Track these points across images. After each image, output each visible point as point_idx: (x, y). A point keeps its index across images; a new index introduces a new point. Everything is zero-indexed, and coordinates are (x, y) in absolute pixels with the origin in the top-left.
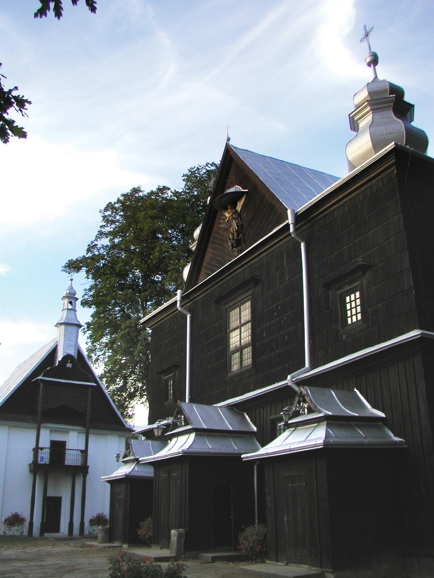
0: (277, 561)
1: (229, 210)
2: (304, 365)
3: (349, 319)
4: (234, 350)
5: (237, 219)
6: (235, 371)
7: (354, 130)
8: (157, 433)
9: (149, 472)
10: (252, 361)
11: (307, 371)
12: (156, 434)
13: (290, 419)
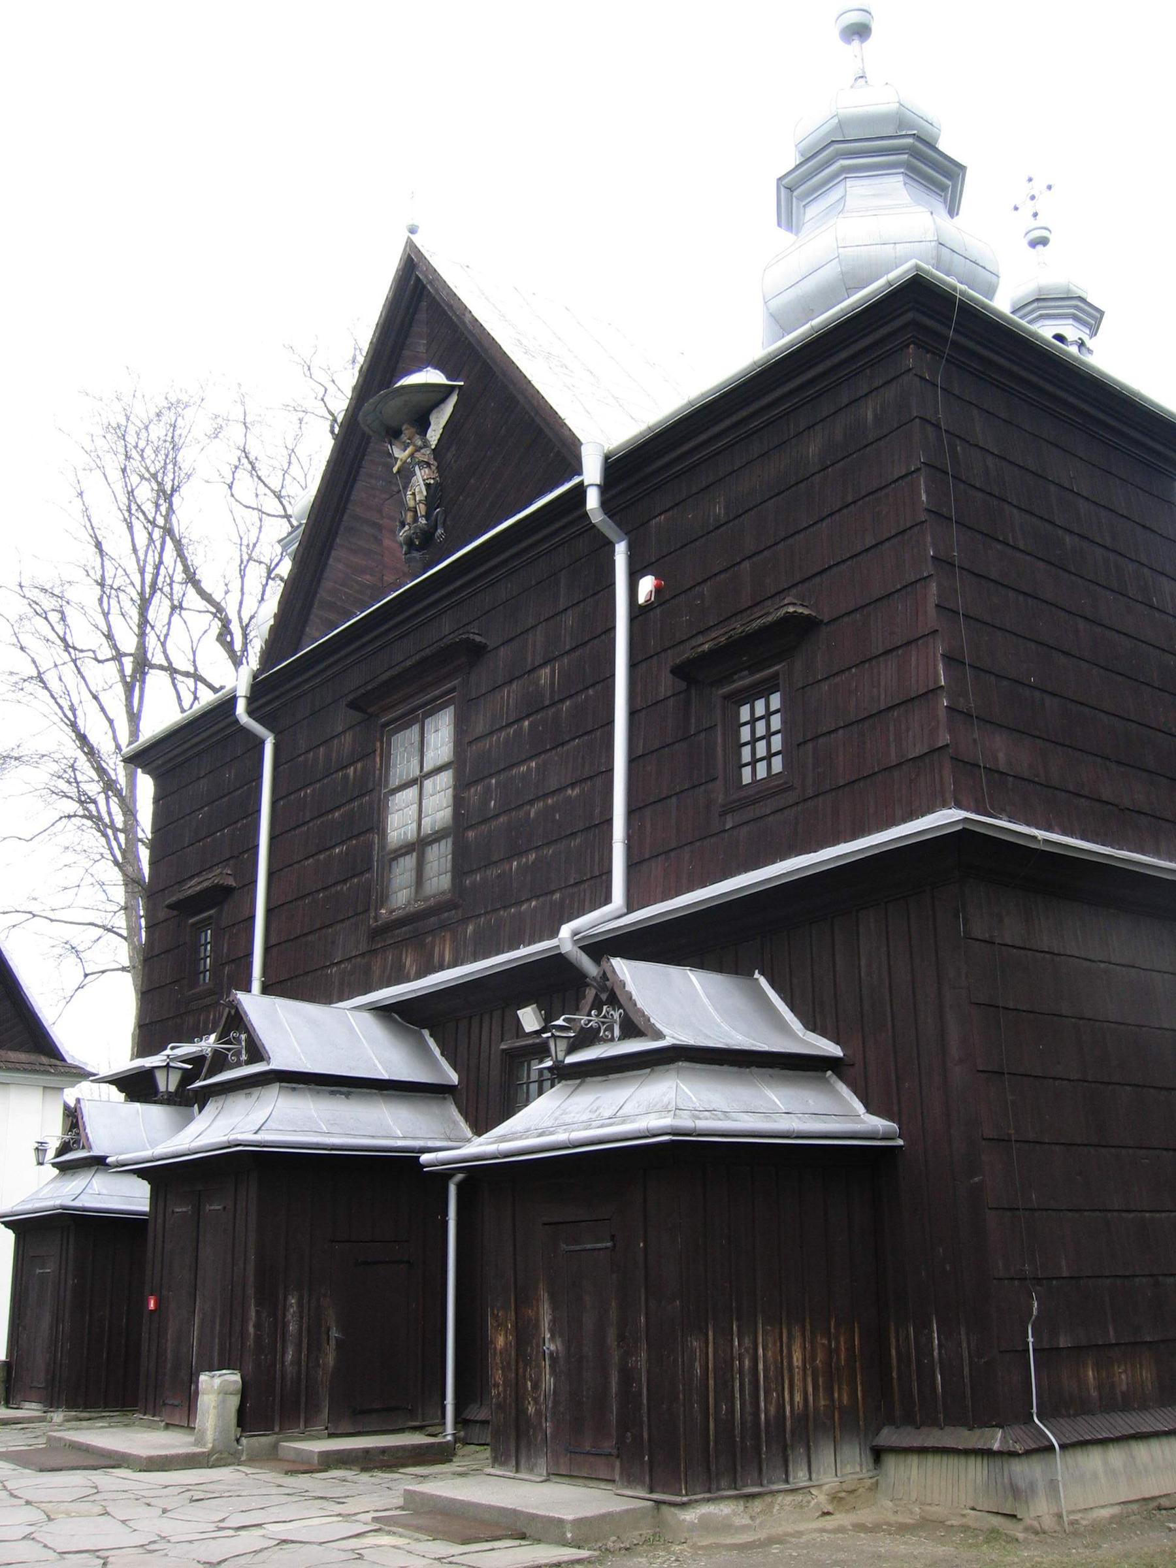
0: (517, 1471)
1: (404, 438)
2: (608, 900)
3: (746, 773)
4: (400, 848)
5: (428, 465)
6: (399, 908)
7: (789, 228)
8: (167, 1083)
9: (134, 1197)
10: (453, 878)
11: (612, 914)
12: (162, 1087)
13: (571, 1050)
